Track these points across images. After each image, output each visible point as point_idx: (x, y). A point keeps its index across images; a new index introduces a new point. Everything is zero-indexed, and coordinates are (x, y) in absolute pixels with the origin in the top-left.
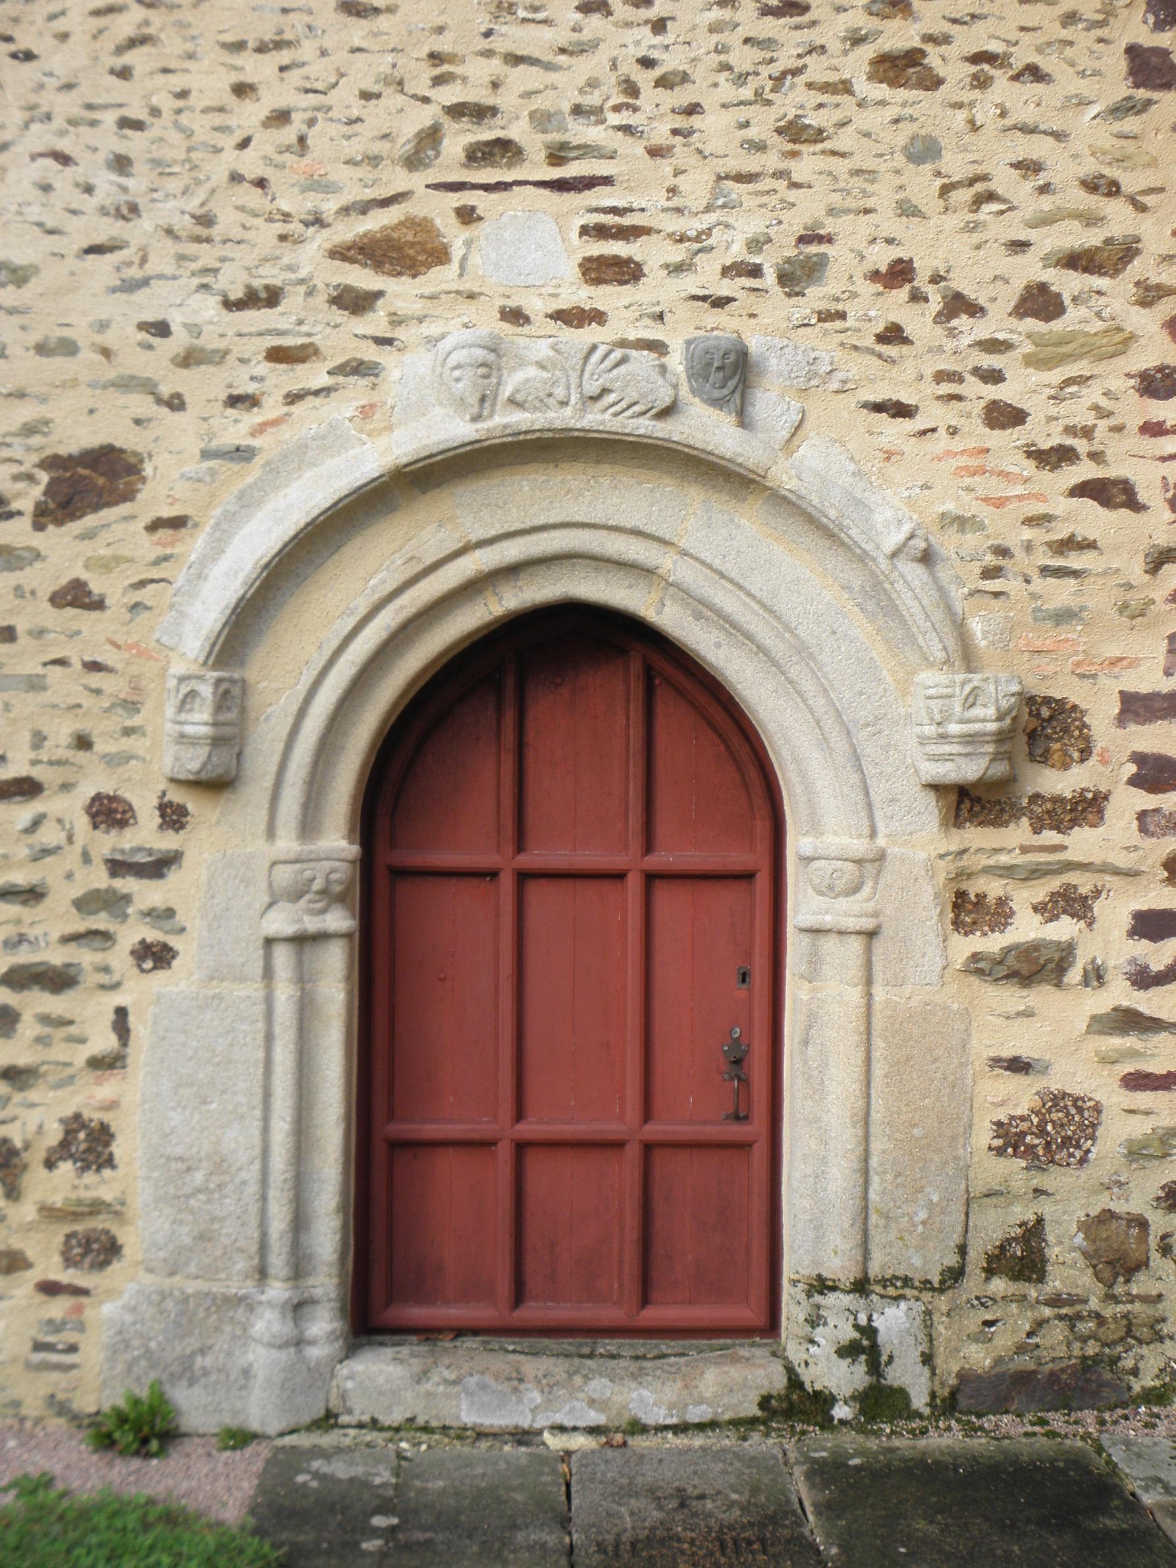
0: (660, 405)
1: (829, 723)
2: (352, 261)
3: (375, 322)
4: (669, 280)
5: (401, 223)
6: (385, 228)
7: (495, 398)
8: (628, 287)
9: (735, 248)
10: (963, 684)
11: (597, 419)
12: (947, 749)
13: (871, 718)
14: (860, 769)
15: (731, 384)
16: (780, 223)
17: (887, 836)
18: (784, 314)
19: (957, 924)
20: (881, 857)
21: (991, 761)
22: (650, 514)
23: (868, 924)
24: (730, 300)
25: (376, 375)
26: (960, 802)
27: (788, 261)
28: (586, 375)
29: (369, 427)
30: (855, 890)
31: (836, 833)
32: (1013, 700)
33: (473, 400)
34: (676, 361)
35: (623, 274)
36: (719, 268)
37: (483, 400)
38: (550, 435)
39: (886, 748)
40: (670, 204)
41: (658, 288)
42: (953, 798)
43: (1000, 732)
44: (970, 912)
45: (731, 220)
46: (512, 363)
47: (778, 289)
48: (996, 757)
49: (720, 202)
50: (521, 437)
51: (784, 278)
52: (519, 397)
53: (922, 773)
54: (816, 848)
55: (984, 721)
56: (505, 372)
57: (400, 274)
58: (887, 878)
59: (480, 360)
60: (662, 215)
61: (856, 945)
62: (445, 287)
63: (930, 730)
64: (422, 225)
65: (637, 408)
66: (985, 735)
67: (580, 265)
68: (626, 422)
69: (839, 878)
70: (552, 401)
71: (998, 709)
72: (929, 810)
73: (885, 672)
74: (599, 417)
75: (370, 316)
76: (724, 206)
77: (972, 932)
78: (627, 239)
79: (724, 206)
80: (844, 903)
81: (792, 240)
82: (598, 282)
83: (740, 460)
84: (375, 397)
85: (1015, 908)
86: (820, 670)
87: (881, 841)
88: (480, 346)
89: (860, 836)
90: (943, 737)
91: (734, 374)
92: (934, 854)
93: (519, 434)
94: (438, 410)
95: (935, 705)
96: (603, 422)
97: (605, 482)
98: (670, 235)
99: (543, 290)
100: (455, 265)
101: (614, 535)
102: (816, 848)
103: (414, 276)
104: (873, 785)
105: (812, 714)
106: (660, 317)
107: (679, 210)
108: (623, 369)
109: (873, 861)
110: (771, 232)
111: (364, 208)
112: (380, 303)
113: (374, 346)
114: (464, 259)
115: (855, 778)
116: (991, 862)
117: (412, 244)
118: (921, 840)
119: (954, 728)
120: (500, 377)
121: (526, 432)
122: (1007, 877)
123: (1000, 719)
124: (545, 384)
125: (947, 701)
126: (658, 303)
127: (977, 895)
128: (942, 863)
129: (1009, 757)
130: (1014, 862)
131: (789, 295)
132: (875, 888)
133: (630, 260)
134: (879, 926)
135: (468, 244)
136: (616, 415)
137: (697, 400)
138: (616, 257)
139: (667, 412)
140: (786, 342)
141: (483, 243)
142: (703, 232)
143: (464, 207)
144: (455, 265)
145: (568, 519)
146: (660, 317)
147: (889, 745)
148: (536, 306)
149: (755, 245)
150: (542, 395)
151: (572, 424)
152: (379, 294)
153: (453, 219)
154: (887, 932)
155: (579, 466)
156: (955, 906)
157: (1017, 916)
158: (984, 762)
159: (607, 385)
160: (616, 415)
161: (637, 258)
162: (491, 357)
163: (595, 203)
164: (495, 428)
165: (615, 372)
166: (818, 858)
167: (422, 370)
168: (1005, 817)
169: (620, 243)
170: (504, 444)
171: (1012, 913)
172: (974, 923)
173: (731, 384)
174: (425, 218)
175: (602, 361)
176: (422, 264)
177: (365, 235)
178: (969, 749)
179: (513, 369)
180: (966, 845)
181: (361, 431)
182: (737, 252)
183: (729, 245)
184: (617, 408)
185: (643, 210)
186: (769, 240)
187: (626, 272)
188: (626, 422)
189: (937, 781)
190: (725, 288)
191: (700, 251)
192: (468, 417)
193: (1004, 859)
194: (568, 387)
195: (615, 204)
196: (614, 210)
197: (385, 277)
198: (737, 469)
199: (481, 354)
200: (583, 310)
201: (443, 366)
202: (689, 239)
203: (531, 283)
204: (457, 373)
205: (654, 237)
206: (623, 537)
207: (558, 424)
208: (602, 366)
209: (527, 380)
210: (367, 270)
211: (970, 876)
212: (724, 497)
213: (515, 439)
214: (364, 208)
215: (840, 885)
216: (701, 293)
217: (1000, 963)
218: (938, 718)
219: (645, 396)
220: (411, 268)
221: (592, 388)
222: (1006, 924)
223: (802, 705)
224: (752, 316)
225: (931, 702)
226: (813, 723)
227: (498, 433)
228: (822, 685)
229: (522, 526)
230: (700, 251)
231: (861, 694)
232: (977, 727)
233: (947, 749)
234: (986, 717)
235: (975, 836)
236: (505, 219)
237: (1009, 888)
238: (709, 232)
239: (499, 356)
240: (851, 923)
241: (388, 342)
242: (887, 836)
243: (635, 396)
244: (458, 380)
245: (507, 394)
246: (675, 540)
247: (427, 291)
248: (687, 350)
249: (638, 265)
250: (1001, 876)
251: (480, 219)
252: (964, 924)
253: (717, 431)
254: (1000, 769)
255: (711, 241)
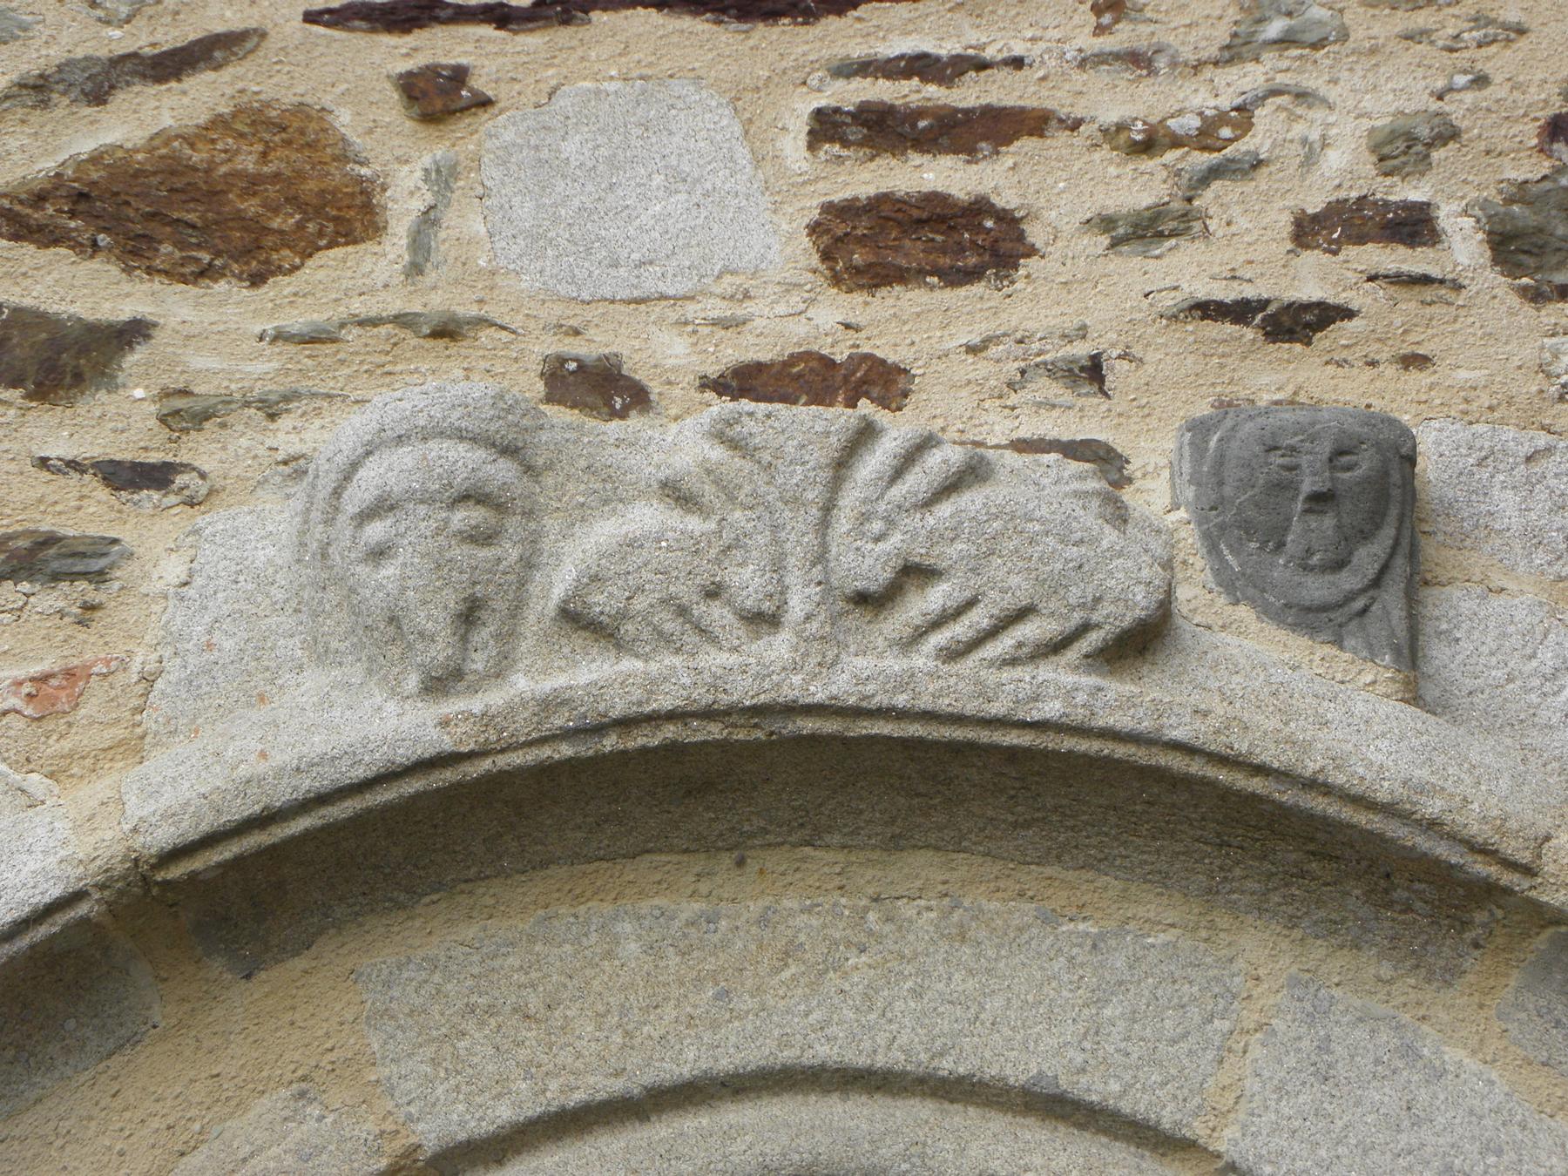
0: (1115, 617)
2: (46, 236)
3: (118, 419)
4: (1115, 263)
5: (219, 123)
6: (164, 137)
7: (516, 610)
8: (978, 288)
9: (1335, 160)
11: (876, 670)
15: (1367, 557)
16: (1481, 81)
18: (1527, 352)
22: (1096, 1030)
24: (1326, 315)
25: (99, 577)
27: (1521, 193)
28: (843, 522)
29: (56, 747)
33: (433, 618)
34: (1158, 495)
35: (961, 249)
36: (1285, 223)
37: (469, 615)
38: (715, 731)
40: (1108, 43)
41: (1071, 290)
45: (1312, 81)
46: (576, 492)
47: (1495, 280)
49: (1275, 28)
50: (610, 743)
51: (1509, 246)
52: (601, 602)
56: (552, 524)
57: (206, 273)
59: (460, 481)
60: (1079, 78)
62: (358, 306)
64: (295, 129)
65: (1030, 631)
67: (814, 229)
68: (992, 677)
70: (717, 614)
74: (894, 664)
75: (98, 402)
76: (1285, 41)
78: (968, 150)
79: (1285, 41)
81: (1530, 134)
82: (876, 277)
83: (1433, 807)
84: (89, 648)
88: (460, 435)
91: (1376, 520)
93: (599, 729)
94: (314, 680)
96: (906, 681)
97: (922, 917)
98: (1114, 134)
99: (691, 309)
100: (397, 242)
101: (964, 1117)
103: (257, 280)
106: (1094, 371)
107: (1138, 60)
108: (971, 500)
110: (1457, 109)
111: (99, 83)
112: (134, 359)
113: (103, 493)
114: (429, 219)
117: (253, 184)
120: (533, 540)
121: (626, 723)
124: (691, 581)
126: (1083, 332)
131: (1535, 296)
133: (980, 207)
135: (443, 178)
136: (953, 654)
137: (1244, 612)
138: (934, 198)
139: (1142, 642)
140: (1542, 440)
141: (492, 173)
142: (1222, 118)
143: (432, 71)
144: (397, 242)
145: (788, 1056)
146: (1094, 371)
148: (666, 353)
149: (1403, 148)
150: (685, 591)
151: (795, 688)
152: (135, 332)
153: (392, 110)
155: (824, 861)
159: (919, 553)
160: (953, 654)
161: (1006, 199)
162: (502, 471)
163: (858, 50)
164: (510, 710)
165: (945, 509)
167: (262, 554)
169: (947, 161)
170: (546, 771)
173: (1367, 557)
174: (301, 109)
175: (898, 474)
176: (285, 240)
177: (96, 159)
179: (583, 514)
181: (27, 763)
182: (1344, 169)
183: (1311, 155)
184: (960, 630)
185: (1017, 63)
186: (1448, 134)
187: (979, 244)
188: (992, 677)
190: (1310, 279)
191: (1214, 173)
192: (412, 682)
194: (778, 565)
195: (927, 46)
196: (920, 66)
197: (158, 284)
198: (1423, 843)
199: (464, 460)
200: (828, 363)
201: (329, 521)
202: (1176, 142)
203: (650, 286)
204: (376, 531)
205: (1059, 140)
206: (998, 1122)
207: (743, 691)
208: (898, 491)
209: (632, 544)
210: (96, 264)
212: (1375, 966)
213: (585, 749)
214: (99, 83)
216: (1227, 293)
219: (1057, 586)
220: (245, 254)
221: (868, 564)
224: (1414, 361)
227: (522, 727)
229: (617, 1086)
230: (1214, 173)
236: (562, 102)
238: (1243, 114)
239: (529, 469)
241: (156, 476)
243: (1020, 589)
244: (379, 554)
245: (558, 592)
246: (1197, 1129)
247: (296, 320)
248: (1198, 448)
249: (1009, 220)
251: (485, 103)
253: (1333, 712)
255: (1256, 142)
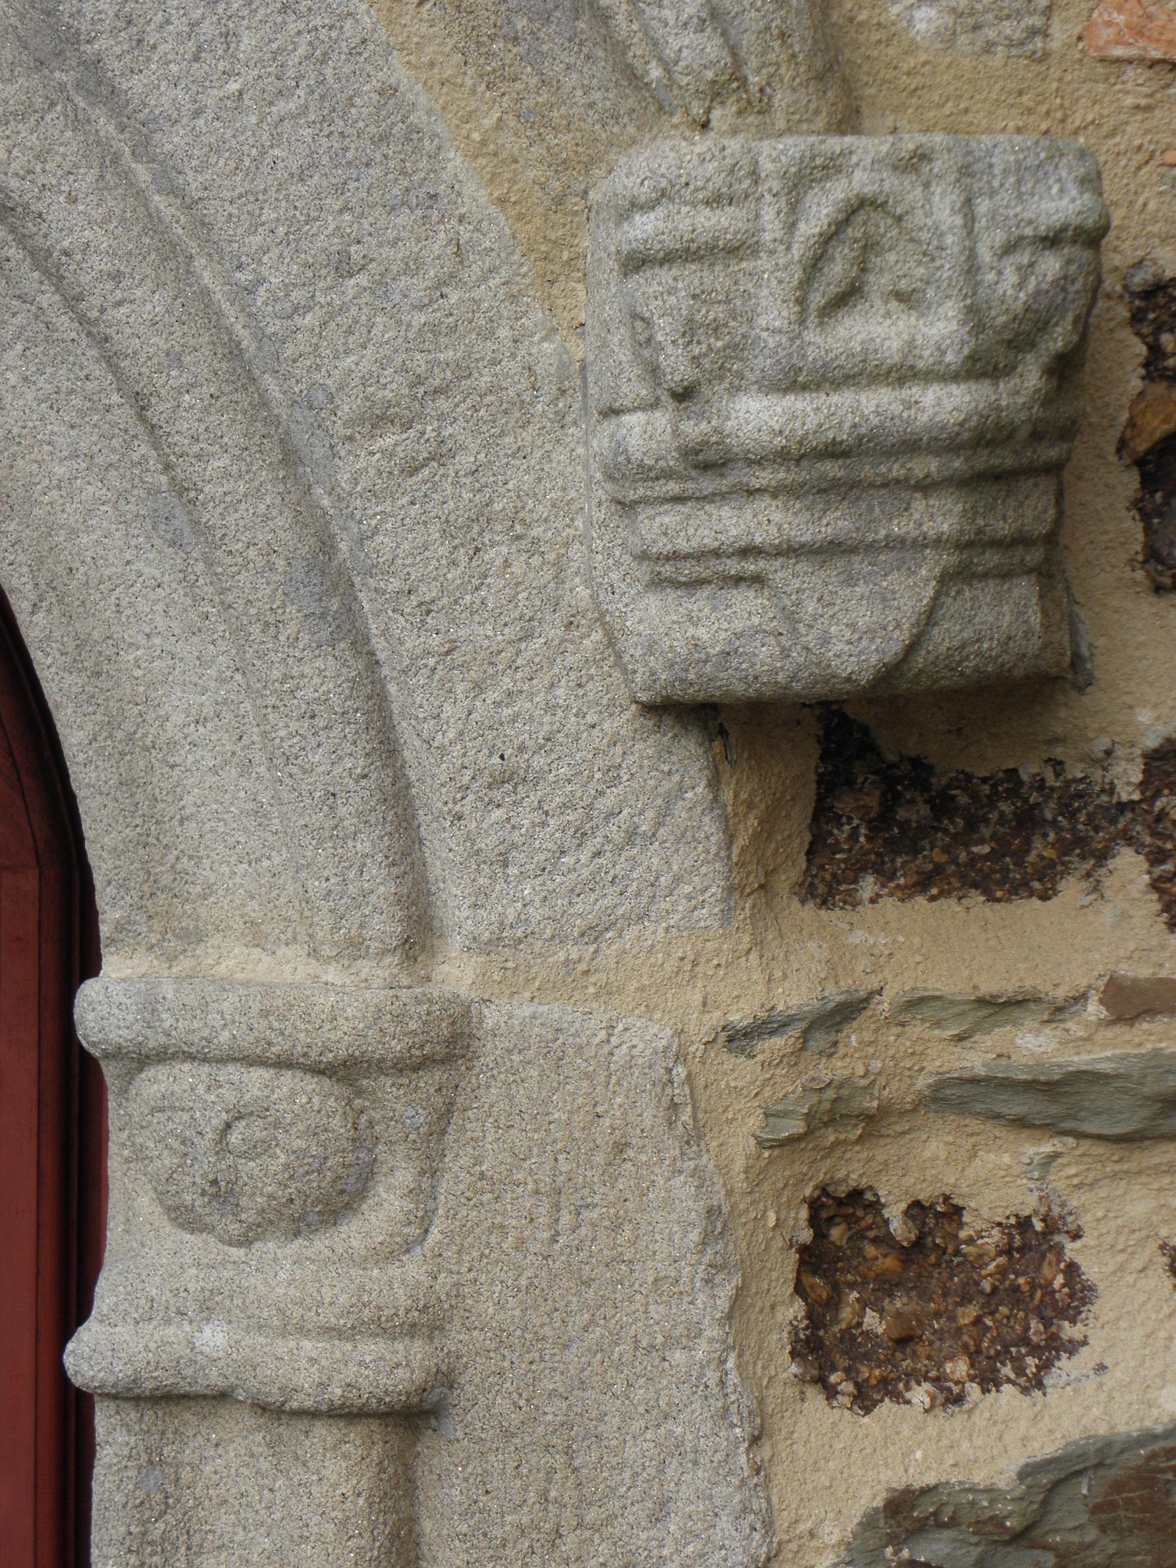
1: (192, 412)
10: (801, 181)
12: (732, 523)
13: (394, 388)
14: (349, 632)
17: (476, 945)
19: (822, 1353)
20: (449, 1047)
21: (946, 579)
23: (384, 1368)
26: (829, 787)
30: (337, 1202)
31: (256, 936)
32: (1051, 265)
39: (470, 531)
42: (799, 768)
43: (985, 436)
44: (887, 1286)
48: (970, 563)
53: (632, 649)
54: (151, 1007)
55: (902, 374)
58: (485, 1141)
61: (337, 1470)
63: (647, 432)
66: (911, 446)
69: (258, 1149)
71: (975, 315)
72: (673, 828)
73: (455, 161)
77: (891, 1389)
80: (283, 1269)
85: (1091, 1270)
86: (143, 149)
87: (456, 973)
89: (354, 948)
90: (709, 465)
92: (702, 1026)
95: (665, 294)
102: (151, 1007)
104: (410, 701)
105: (111, 361)
109: (411, 1066)
115: (323, 675)
116: (975, 1059)
118: (640, 966)
119: (755, 416)
122: (1052, 1128)
123: (979, 367)
125: (716, 278)
127: (917, 1210)
128: (742, 1071)
129: (1045, 560)
130: (1080, 1060)
132: (424, 1195)
134: (446, 1378)
147: (482, 517)
154: (482, 1406)
156: (813, 1259)
157: (1102, 1308)
158: (910, 590)
166: (163, 1056)
168: (1041, 849)
171: (1080, 1294)
172: (904, 1341)
178: (836, 523)
180: (857, 980)
189: (698, 683)
193: (1033, 1045)
211: (874, 1123)
215: (262, 1179)
217: (1022, 1537)
218: (677, 365)
222: (1054, 1348)
223: (64, 323)
225: (651, 286)
226: (124, 415)
228: (154, 224)
231: (343, 267)
232: (873, 405)
233: (732, 523)
234: (915, 355)
235: (912, 944)
237: (1058, 1180)
240: (307, 1367)
242: (476, 945)
250: (1021, 1123)
252: (854, 1344)
254: (998, 622)
